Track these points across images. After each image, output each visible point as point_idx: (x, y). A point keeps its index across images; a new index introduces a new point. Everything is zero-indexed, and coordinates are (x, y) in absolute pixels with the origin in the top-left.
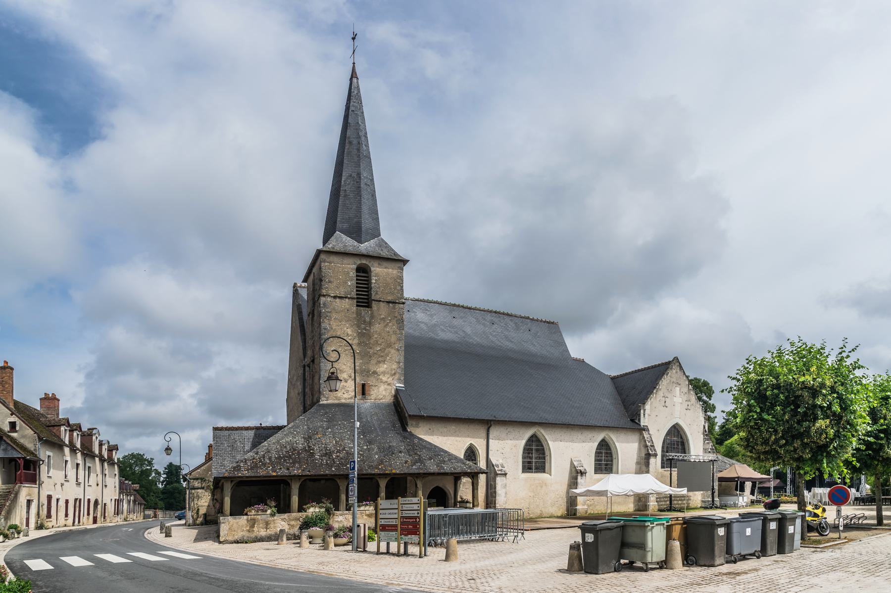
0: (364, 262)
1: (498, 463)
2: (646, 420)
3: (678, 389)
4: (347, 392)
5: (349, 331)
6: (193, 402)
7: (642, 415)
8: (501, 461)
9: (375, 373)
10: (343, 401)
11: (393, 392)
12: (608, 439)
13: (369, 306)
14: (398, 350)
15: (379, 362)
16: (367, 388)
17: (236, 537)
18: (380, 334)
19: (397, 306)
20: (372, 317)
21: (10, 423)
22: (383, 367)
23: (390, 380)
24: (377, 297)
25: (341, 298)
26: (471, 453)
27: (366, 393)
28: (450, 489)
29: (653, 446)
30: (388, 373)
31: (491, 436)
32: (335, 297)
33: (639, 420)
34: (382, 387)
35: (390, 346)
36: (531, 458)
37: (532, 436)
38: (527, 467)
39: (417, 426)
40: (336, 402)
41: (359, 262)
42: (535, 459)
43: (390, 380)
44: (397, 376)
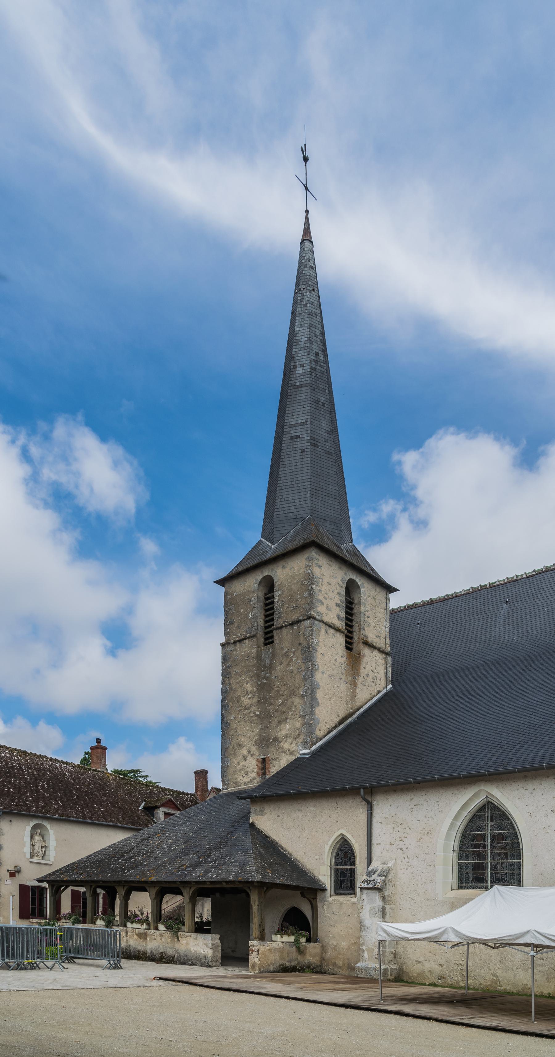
4: (247, 773)
5: (249, 687)
6: (123, 944)
9: (276, 739)
15: (280, 722)
18: (282, 679)
22: (286, 728)
25: (240, 641)
30: (290, 737)
32: (235, 643)
35: (293, 693)
36: (482, 856)
39: (262, 813)
40: (236, 789)
41: (259, 576)
43: (293, 747)
44: (300, 740)
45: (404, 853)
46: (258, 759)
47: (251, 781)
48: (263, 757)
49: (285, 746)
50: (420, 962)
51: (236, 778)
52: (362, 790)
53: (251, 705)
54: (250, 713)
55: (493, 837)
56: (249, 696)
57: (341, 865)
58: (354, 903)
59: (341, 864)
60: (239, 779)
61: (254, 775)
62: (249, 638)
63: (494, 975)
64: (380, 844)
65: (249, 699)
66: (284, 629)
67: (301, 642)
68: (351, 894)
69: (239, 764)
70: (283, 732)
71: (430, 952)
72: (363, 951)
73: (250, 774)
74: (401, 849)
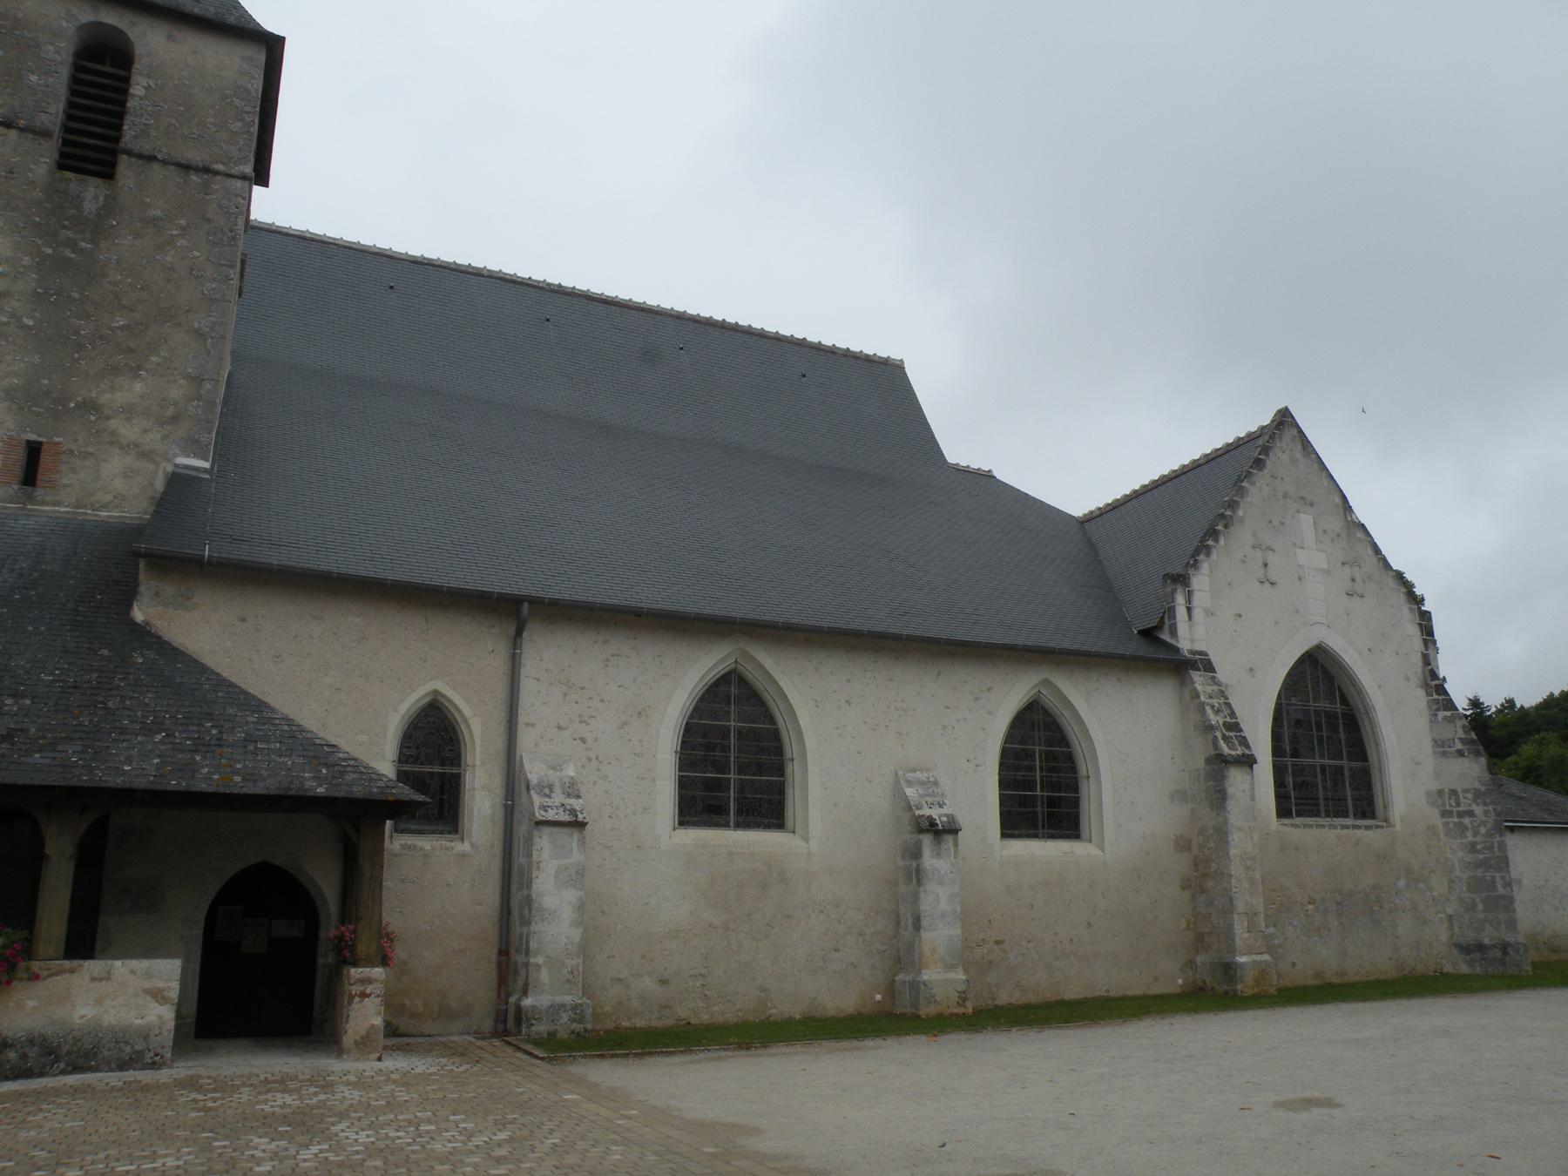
1: (553, 776)
2: (1200, 631)
3: (1306, 519)
7: (1181, 612)
8: (571, 772)
9: (89, 406)
11: (160, 485)
12: (1049, 700)
13: (105, 170)
15: (115, 370)
16: (45, 459)
19: (218, 184)
20: (111, 206)
21: (29, 442)
22: (133, 390)
23: (153, 439)
24: (146, 147)
26: (433, 737)
27: (43, 475)
28: (324, 880)
29: (1235, 727)
31: (529, 668)
33: (1173, 631)
36: (722, 767)
37: (724, 679)
38: (700, 803)
42: (734, 770)
43: (153, 439)
45: (588, 749)
46: (11, 437)
48: (32, 437)
49: (123, 431)
50: (619, 980)
52: (526, 606)
55: (740, 734)
57: (415, 762)
58: (463, 855)
59: (416, 760)
62: (22, 130)
63: (763, 989)
66: (156, 166)
70: (121, 397)
72: (538, 967)
74: (583, 740)
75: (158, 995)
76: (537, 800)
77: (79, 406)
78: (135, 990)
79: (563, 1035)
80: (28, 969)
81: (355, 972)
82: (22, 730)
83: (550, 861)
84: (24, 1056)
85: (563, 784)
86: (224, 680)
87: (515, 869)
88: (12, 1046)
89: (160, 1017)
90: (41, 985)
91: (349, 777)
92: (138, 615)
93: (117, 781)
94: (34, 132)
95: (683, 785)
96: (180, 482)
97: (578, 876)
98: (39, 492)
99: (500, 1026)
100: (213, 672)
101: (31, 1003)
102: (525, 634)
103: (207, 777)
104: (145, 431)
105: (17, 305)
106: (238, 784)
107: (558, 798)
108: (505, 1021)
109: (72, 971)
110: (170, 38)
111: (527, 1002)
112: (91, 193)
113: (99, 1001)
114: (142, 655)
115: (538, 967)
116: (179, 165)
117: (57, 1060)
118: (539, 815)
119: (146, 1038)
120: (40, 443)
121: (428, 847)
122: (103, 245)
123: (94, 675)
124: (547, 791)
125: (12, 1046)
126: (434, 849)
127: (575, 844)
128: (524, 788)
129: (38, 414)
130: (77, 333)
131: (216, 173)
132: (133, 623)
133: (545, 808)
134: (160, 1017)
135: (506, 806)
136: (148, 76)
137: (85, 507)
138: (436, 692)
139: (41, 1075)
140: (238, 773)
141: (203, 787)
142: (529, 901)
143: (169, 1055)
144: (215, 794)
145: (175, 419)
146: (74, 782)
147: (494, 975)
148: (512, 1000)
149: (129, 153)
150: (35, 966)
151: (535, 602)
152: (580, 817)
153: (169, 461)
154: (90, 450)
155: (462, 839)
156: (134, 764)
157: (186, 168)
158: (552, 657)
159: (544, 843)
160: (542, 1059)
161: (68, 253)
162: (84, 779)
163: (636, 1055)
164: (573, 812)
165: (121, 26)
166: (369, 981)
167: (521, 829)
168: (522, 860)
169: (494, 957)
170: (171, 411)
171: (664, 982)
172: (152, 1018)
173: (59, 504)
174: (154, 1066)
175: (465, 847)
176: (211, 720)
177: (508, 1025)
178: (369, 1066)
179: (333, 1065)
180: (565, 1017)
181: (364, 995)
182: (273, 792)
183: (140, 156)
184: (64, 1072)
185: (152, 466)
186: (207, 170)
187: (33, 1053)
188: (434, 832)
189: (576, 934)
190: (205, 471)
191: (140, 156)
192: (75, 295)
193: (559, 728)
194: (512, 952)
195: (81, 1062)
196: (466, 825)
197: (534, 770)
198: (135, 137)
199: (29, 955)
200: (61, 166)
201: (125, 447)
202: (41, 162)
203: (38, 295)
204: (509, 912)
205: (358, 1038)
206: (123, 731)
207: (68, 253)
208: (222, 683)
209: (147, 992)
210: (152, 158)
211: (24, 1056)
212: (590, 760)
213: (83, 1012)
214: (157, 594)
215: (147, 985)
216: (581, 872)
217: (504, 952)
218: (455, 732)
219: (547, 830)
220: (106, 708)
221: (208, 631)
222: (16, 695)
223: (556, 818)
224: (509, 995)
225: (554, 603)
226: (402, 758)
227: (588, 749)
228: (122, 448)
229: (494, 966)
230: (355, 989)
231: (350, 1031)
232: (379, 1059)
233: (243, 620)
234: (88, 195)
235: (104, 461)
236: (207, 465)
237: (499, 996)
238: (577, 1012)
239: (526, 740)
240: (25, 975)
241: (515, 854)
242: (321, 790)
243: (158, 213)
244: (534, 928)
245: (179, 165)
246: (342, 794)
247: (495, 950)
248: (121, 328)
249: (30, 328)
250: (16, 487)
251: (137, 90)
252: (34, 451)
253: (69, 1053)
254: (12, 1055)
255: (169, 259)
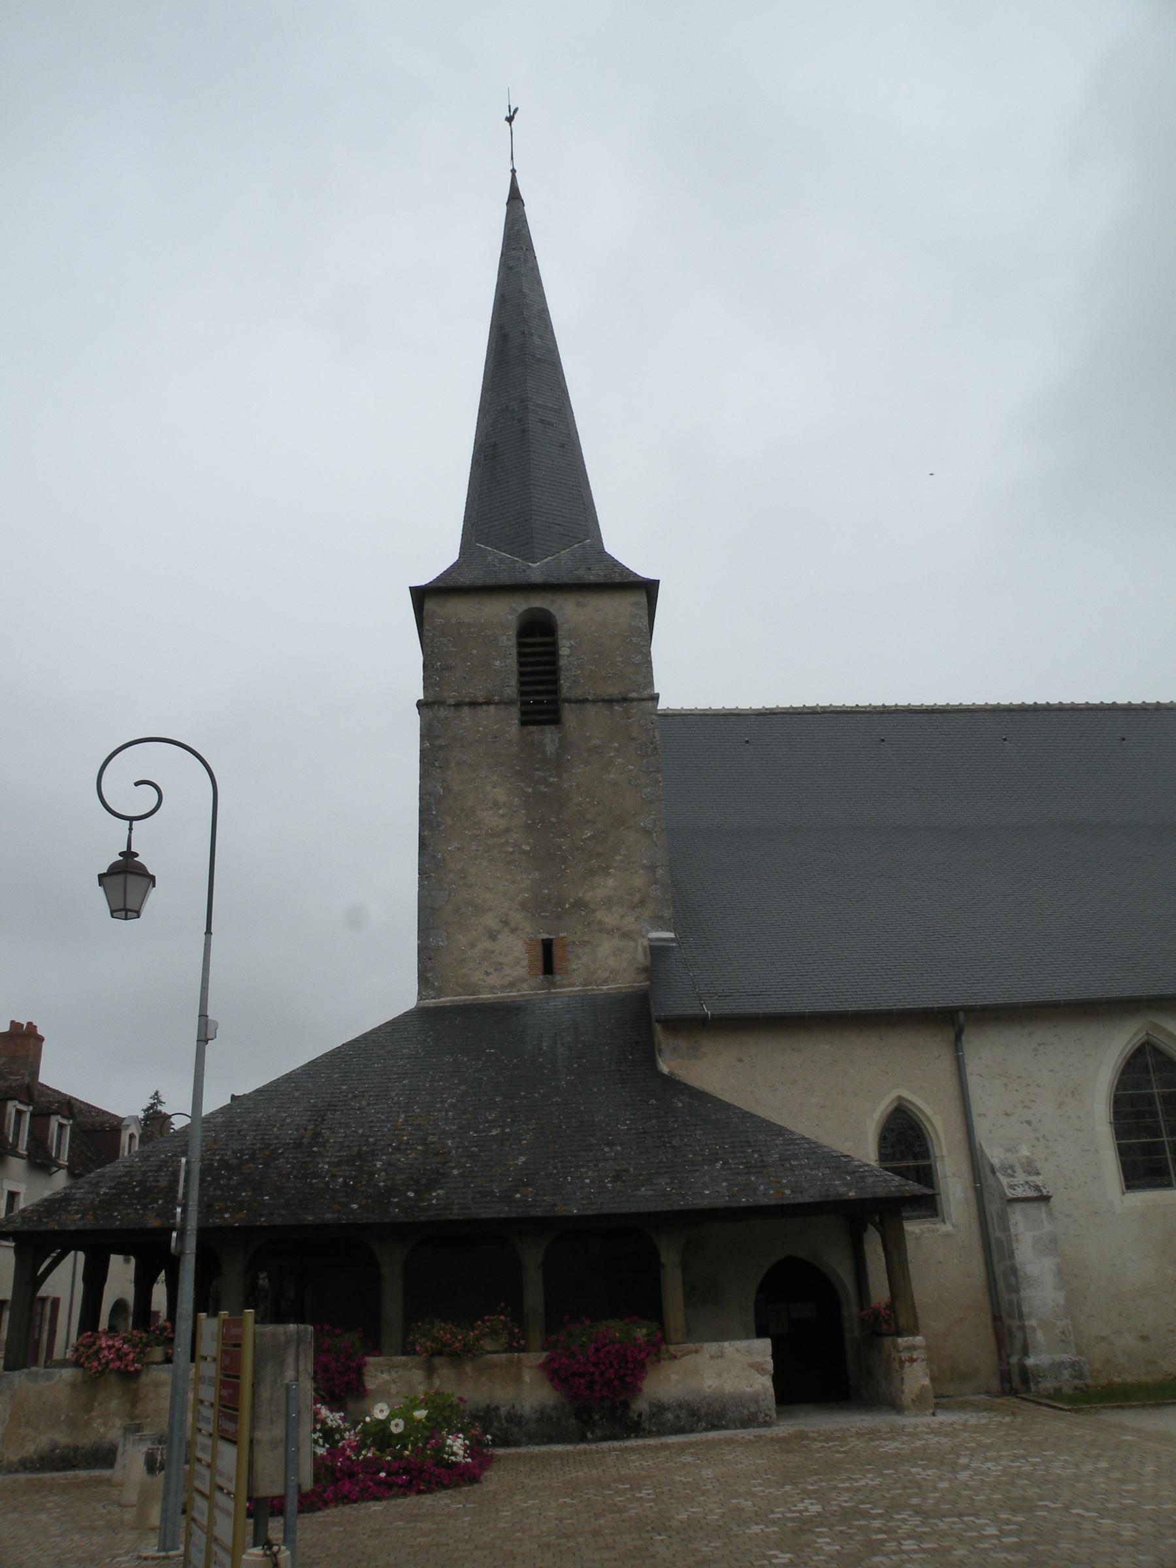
0: (537, 602)
1: (1012, 1158)
4: (499, 967)
5: (500, 794)
8: (1025, 1151)
9: (580, 904)
10: (486, 996)
14: (647, 832)
15: (592, 872)
16: (557, 951)
17: (30, 1449)
19: (635, 708)
20: (564, 746)
21: (543, 940)
22: (607, 886)
24: (578, 693)
25: (474, 704)
26: (904, 1136)
27: (557, 964)
31: (972, 1067)
32: (458, 705)
34: (606, 947)
36: (1154, 1131)
41: (521, 605)
43: (629, 922)
46: (531, 939)
47: (512, 985)
48: (545, 936)
49: (607, 920)
50: (1103, 1338)
51: (466, 975)
52: (961, 1014)
53: (508, 830)
54: (507, 843)
56: (501, 812)
58: (947, 1235)
60: (473, 979)
61: (520, 971)
62: (497, 704)
64: (984, 1115)
65: (502, 816)
66: (589, 706)
67: (635, 735)
68: (932, 1216)
69: (473, 945)
70: (600, 893)
71: (1120, 1315)
73: (507, 970)
74: (1029, 1123)
75: (759, 1368)
76: (1004, 1180)
77: (573, 905)
78: (738, 1366)
79: (1067, 1390)
80: (667, 1351)
81: (902, 1341)
82: (624, 1170)
83: (1026, 1234)
84: (678, 1417)
85: (1022, 1164)
86: (747, 1113)
87: (993, 1242)
88: (668, 1409)
89: (763, 1385)
90: (677, 1362)
91: (870, 1180)
92: (664, 1068)
93: (704, 1203)
94: (505, 704)
95: (1124, 1152)
96: (657, 951)
97: (1051, 1245)
98: (558, 978)
99: (1007, 1386)
100: (735, 1107)
101: (674, 1377)
102: (963, 1038)
103: (765, 1194)
104: (623, 917)
105: (516, 836)
106: (789, 1196)
107: (1021, 1177)
108: (1010, 1380)
109: (697, 1352)
110: (578, 604)
111: (1030, 1361)
112: (548, 738)
113: (719, 1375)
114: (681, 1101)
115: (1033, 1329)
116: (605, 701)
117: (699, 1420)
118: (1010, 1194)
119: (757, 1402)
120: (551, 940)
121: (917, 1231)
122: (565, 776)
123: (654, 1121)
124: (1009, 1171)
125: (668, 1409)
126: (922, 1232)
127: (1044, 1216)
128: (988, 1170)
129: (546, 917)
130: (560, 848)
131: (632, 700)
132: (661, 1075)
133: (1012, 1187)
134: (763, 1385)
135: (975, 1188)
136: (570, 638)
137: (591, 984)
138: (900, 1098)
139: (692, 1431)
140: (785, 1187)
141: (765, 1201)
142: (1014, 1271)
143: (775, 1415)
144: (776, 1206)
145: (642, 902)
146: (676, 1208)
147: (992, 1339)
148: (1014, 1360)
149: (569, 701)
150: (672, 1348)
151: (969, 1010)
152: (1044, 1192)
153: (643, 937)
154: (586, 939)
155: (944, 1221)
156: (711, 1189)
157: (609, 701)
158: (990, 1055)
159: (1018, 1218)
160: (1069, 1410)
161: (544, 789)
162: (681, 1204)
163: (1151, 1406)
164: (1037, 1188)
165: (545, 606)
166: (913, 1348)
167: (993, 1208)
168: (999, 1234)
169: (989, 1323)
170: (638, 897)
171: (1144, 1338)
172: (757, 1386)
173: (573, 985)
174: (766, 1424)
175: (947, 1228)
176: (750, 1146)
177: (1015, 1384)
178: (926, 1420)
179: (906, 1421)
180: (1066, 1374)
181: (912, 1360)
182: (818, 1200)
183: (577, 701)
184: (706, 1430)
185: (632, 944)
186: (625, 700)
187: (683, 1414)
188: (919, 1217)
189: (1060, 1297)
190: (672, 940)
191: (577, 701)
192: (553, 820)
193: (1007, 1114)
194: (1004, 1317)
195: (715, 1422)
196: (945, 1208)
197: (995, 1155)
198: (570, 688)
199: (665, 1340)
200: (524, 723)
201: (610, 932)
202: (508, 723)
203: (529, 825)
204: (995, 1280)
205: (913, 1396)
206: (692, 1163)
207: (544, 789)
208: (748, 1116)
209: (752, 1366)
210: (585, 701)
211: (678, 1417)
212: (1038, 1139)
213: (710, 1383)
214: (674, 1049)
215: (750, 1361)
216: (1054, 1241)
217: (997, 1318)
218: (920, 1129)
219: (1018, 1206)
220: (673, 1147)
221: (716, 1071)
222: (610, 1144)
223: (1025, 1195)
224: (1009, 1356)
225: (985, 1009)
226: (883, 1157)
227: (1035, 1130)
228: (608, 933)
229: (991, 1331)
230: (904, 1355)
231: (906, 1391)
232: (934, 1414)
233: (741, 1060)
234: (547, 741)
235: (598, 945)
236: (672, 935)
237: (1000, 1358)
238: (1077, 1370)
239: (981, 1128)
240: (666, 1356)
241: (991, 1230)
242: (852, 1194)
243: (597, 742)
244: (1023, 1294)
245: (605, 701)
246: (869, 1196)
247: (990, 1316)
248: (589, 838)
249: (528, 852)
250: (541, 977)
251: (564, 651)
252: (548, 947)
253: (707, 1414)
254: (670, 1416)
255: (612, 776)
